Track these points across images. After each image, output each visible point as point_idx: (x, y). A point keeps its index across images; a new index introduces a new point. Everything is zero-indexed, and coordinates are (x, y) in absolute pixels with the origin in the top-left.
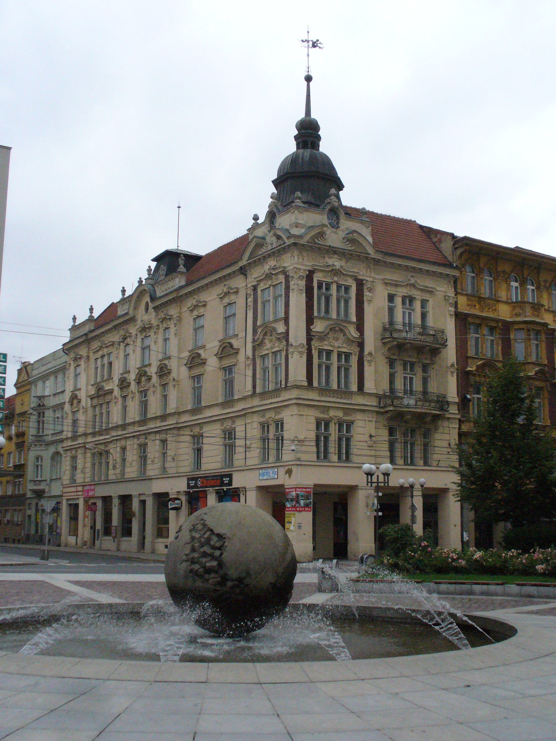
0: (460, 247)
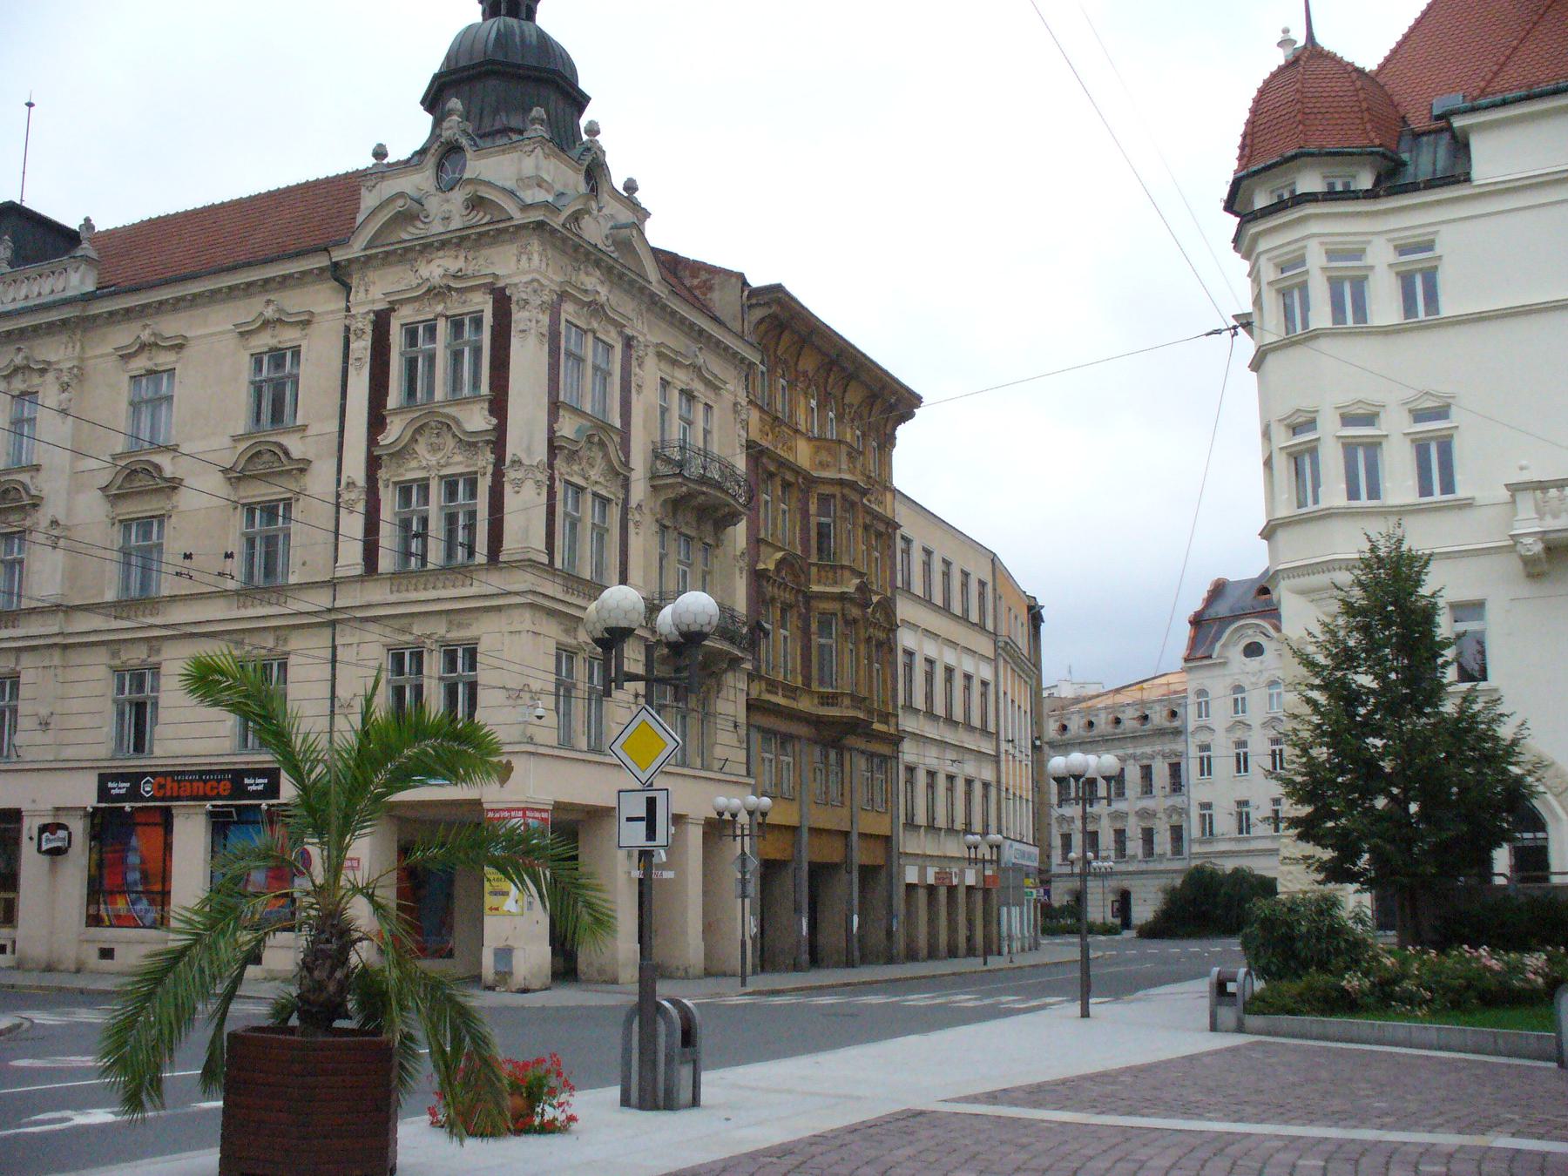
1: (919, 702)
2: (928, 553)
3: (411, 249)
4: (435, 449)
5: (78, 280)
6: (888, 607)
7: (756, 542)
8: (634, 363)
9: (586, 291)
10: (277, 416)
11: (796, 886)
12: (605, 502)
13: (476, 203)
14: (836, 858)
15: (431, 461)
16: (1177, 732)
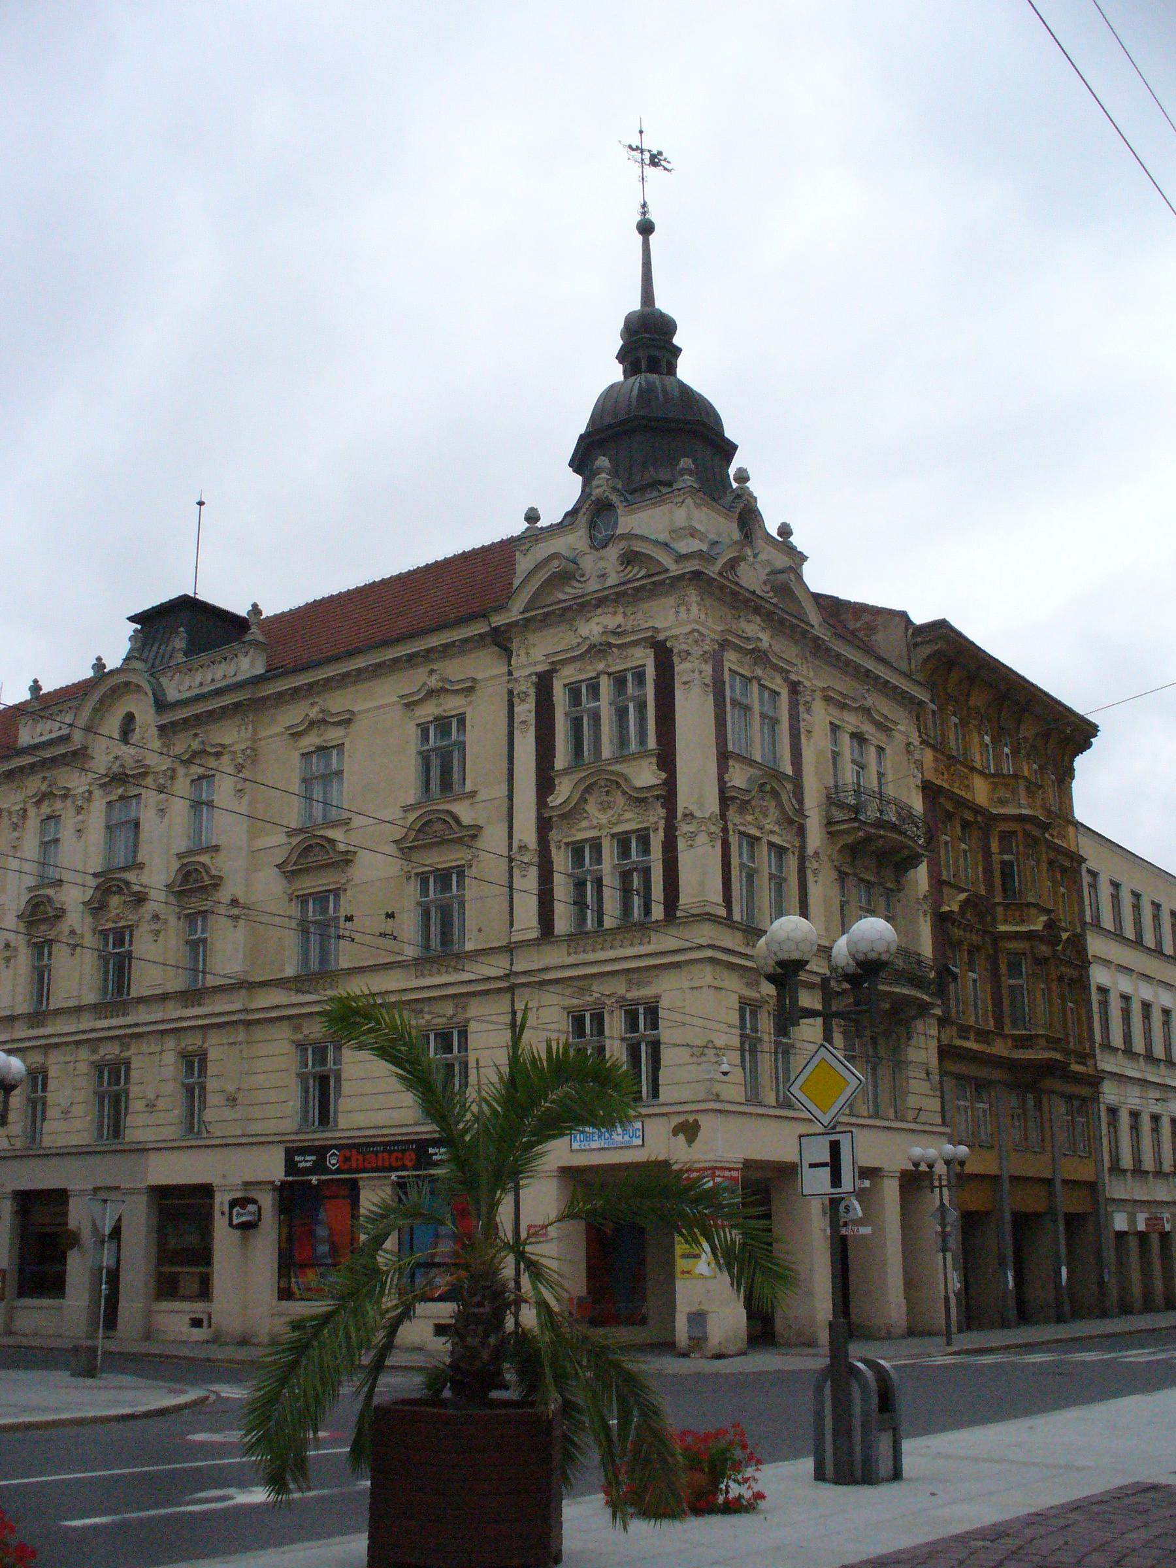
0: (928, 642)
1: (1117, 1040)
2: (1116, 885)
3: (569, 608)
4: (604, 807)
5: (249, 665)
6: (1078, 944)
7: (938, 884)
8: (801, 708)
9: (748, 639)
10: (446, 785)
11: (999, 1239)
12: (780, 851)
13: (630, 558)
14: (1041, 1206)
15: (601, 820)
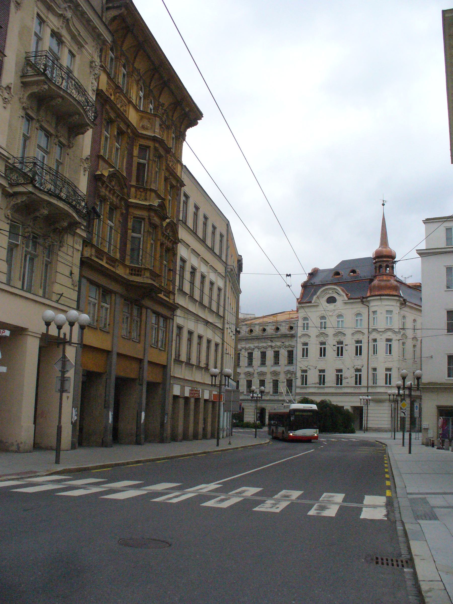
1: (187, 288)
6: (173, 227)
11: (105, 391)
16: (293, 336)
